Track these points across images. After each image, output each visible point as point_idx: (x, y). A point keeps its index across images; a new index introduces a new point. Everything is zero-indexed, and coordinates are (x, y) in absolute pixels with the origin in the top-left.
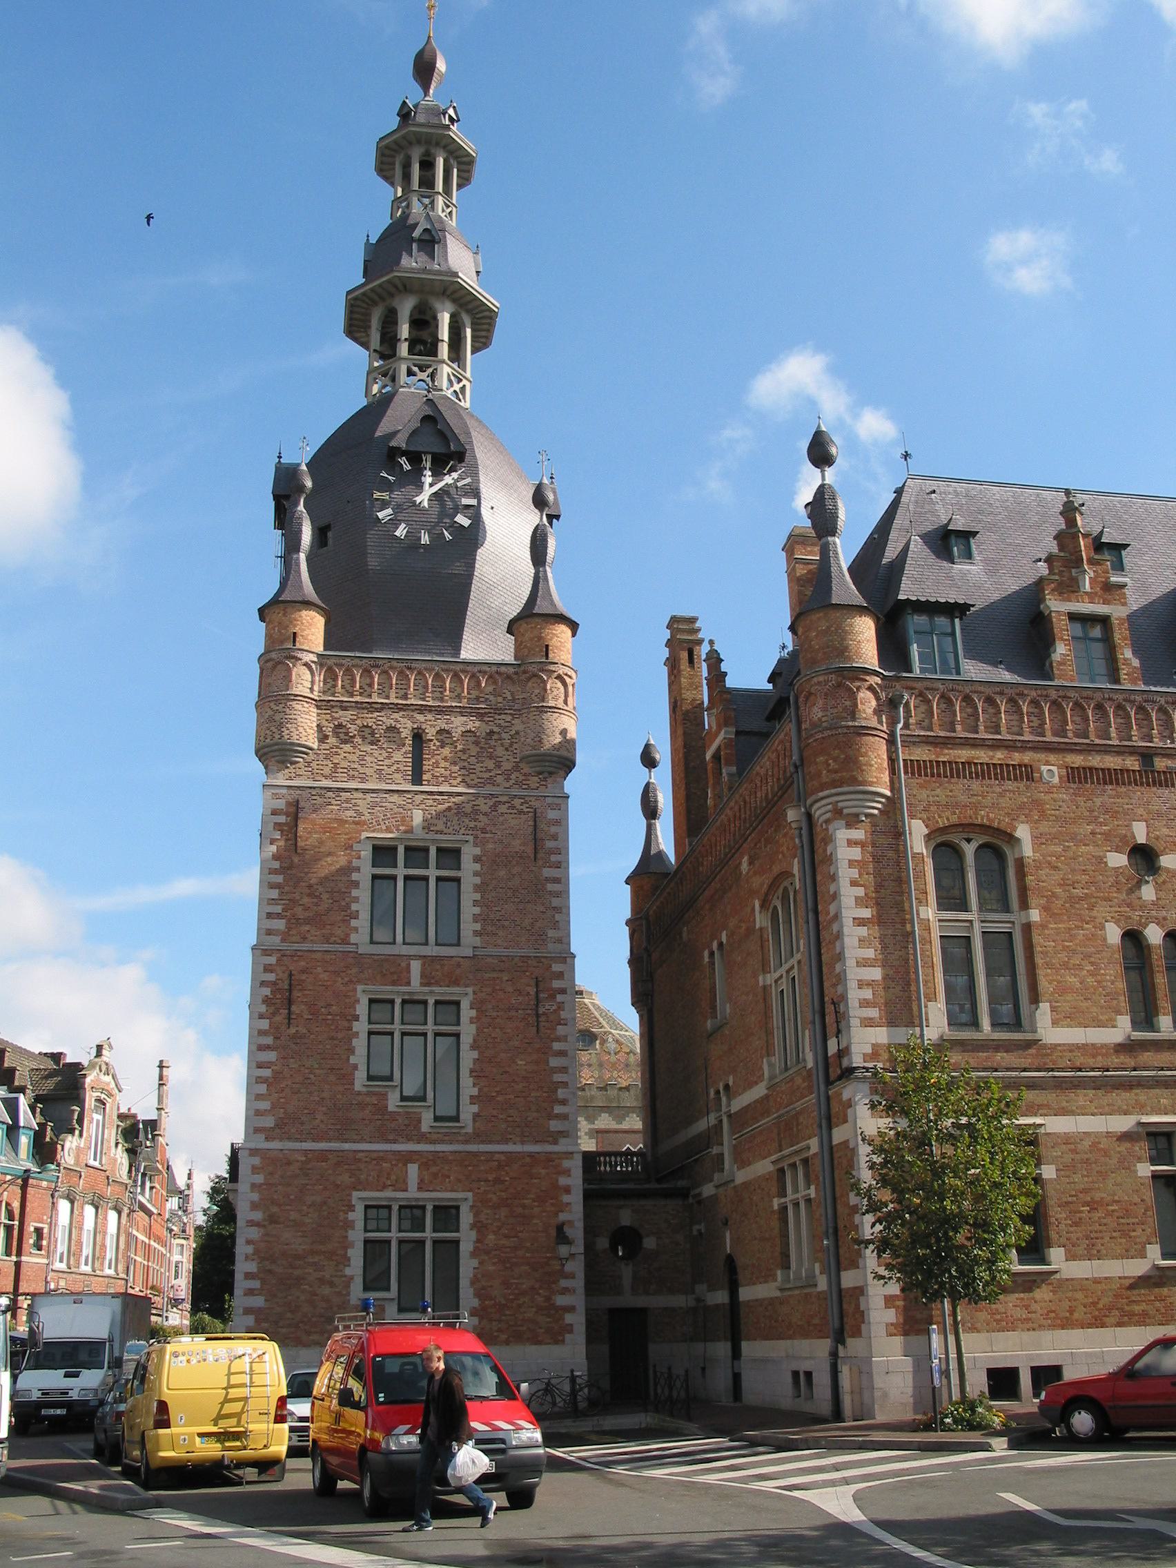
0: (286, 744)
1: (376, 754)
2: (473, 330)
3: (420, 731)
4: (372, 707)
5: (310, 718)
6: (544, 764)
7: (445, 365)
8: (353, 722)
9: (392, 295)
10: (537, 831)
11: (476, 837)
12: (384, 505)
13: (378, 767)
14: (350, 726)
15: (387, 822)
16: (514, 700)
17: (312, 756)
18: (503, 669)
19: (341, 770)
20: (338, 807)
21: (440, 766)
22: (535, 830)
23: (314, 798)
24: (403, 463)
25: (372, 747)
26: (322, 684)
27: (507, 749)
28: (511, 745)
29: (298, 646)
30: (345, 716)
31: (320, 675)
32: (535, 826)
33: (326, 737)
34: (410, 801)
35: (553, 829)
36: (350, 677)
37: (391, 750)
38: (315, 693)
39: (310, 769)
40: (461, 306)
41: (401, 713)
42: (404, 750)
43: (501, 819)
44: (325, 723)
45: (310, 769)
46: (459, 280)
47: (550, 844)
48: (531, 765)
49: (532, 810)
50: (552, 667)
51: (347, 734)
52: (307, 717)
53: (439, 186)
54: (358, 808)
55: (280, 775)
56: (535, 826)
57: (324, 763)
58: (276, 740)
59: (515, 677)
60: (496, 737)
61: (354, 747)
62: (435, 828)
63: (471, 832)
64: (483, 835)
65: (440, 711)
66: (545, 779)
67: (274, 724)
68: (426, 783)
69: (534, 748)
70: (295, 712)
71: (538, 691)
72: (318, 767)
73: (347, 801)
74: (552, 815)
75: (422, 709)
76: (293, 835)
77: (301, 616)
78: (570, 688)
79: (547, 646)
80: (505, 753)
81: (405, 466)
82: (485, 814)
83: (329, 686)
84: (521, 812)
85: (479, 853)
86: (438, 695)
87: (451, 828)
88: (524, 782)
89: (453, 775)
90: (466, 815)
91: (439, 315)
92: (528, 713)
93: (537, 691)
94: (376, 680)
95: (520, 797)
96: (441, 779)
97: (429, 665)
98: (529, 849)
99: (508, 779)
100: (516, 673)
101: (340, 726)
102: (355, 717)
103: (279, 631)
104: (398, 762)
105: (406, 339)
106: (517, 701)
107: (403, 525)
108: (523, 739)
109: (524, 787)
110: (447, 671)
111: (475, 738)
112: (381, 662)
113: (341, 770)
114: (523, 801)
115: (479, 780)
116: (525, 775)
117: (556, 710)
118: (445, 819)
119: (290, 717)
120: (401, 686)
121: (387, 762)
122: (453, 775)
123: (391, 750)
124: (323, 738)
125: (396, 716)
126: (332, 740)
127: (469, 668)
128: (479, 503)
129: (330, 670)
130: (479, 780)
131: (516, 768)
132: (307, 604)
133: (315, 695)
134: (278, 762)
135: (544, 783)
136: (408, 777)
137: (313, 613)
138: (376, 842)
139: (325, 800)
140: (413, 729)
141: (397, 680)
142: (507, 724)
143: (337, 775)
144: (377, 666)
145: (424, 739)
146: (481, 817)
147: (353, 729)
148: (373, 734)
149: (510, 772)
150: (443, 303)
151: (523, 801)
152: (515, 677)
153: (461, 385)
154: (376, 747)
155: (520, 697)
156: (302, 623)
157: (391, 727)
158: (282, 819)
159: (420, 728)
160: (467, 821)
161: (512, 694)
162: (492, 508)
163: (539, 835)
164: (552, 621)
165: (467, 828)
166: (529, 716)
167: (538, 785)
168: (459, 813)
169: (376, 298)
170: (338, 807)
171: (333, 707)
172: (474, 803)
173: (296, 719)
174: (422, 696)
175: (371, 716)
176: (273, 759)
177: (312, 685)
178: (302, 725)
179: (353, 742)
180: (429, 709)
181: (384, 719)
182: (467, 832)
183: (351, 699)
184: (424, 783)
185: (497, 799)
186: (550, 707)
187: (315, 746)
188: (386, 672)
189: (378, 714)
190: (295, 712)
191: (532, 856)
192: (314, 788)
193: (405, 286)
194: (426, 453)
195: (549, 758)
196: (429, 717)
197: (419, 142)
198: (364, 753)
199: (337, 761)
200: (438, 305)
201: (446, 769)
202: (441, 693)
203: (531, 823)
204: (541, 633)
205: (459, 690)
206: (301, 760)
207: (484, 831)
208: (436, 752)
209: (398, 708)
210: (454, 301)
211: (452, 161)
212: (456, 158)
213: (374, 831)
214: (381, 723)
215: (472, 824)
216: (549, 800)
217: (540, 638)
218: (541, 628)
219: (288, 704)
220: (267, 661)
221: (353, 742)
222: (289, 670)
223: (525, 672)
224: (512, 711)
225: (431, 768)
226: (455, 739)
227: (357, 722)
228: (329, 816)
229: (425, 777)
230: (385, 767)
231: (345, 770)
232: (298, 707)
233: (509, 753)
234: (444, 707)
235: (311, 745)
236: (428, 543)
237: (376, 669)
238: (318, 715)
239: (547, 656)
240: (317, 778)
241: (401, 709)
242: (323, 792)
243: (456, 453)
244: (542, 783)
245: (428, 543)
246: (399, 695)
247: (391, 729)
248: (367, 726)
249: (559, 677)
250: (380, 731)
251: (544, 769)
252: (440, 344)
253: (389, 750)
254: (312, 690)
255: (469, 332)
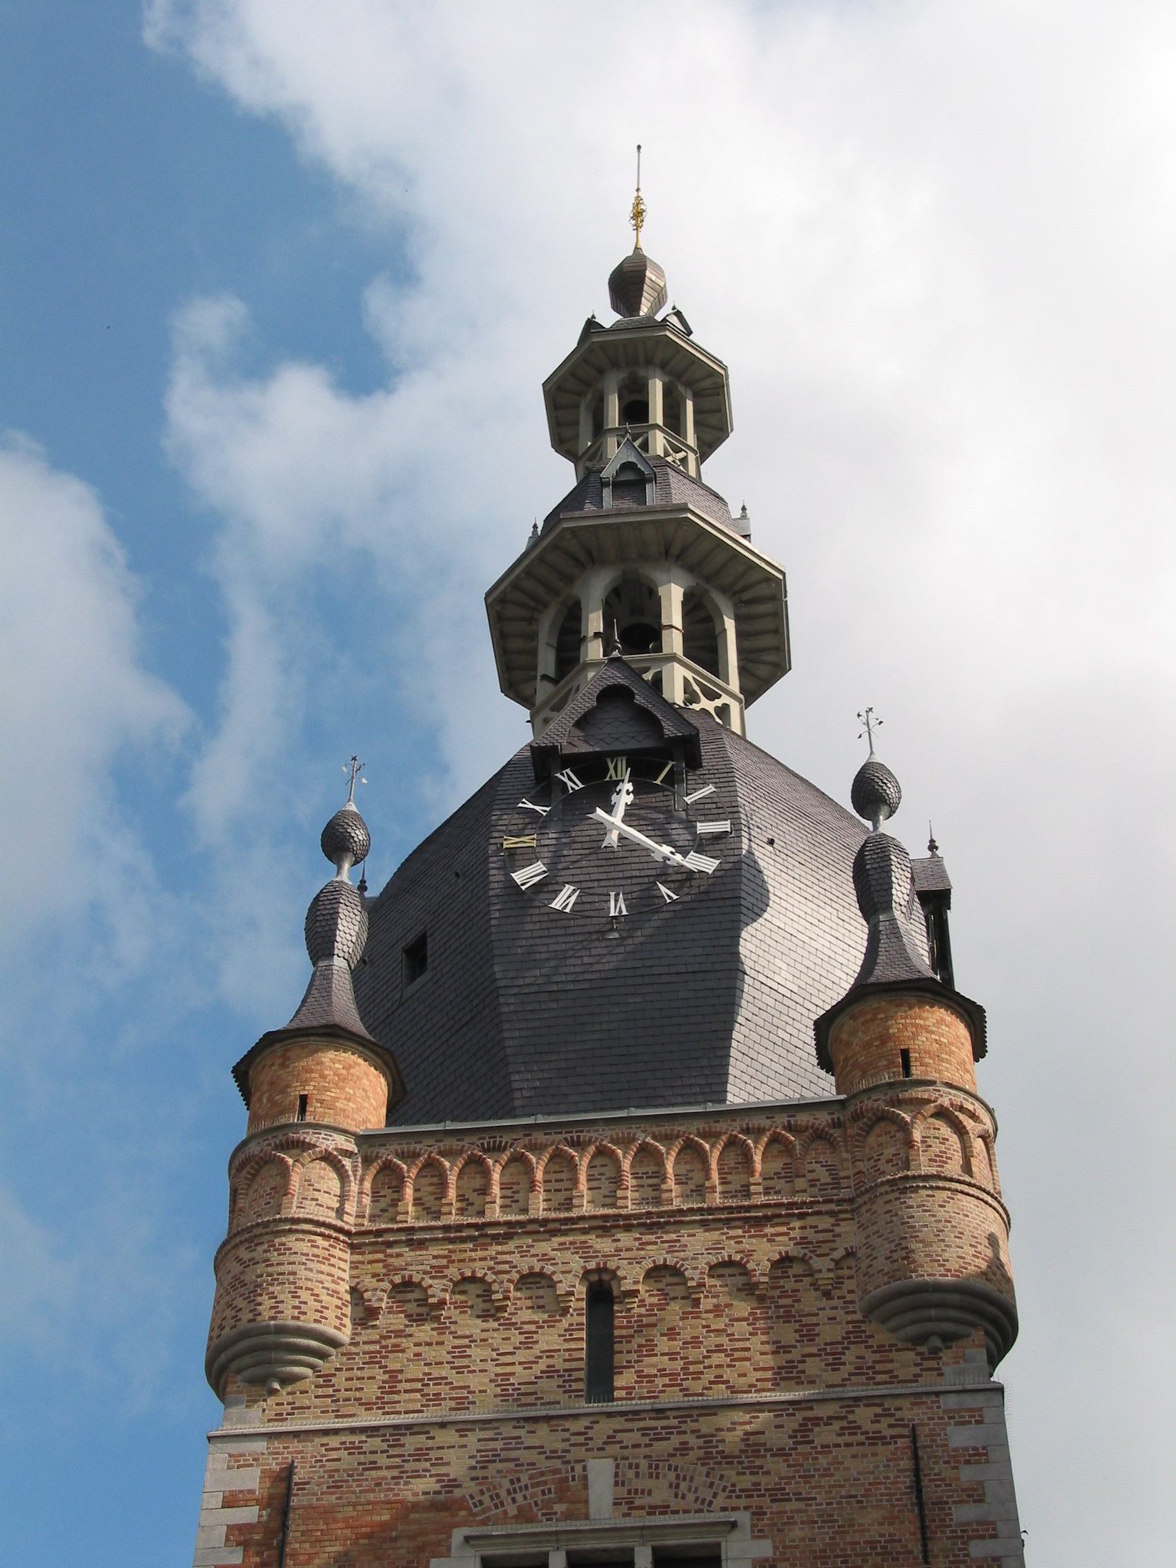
0: (266, 1331)
1: (496, 1338)
2: (738, 619)
3: (606, 1277)
4: (483, 1234)
5: (334, 1271)
6: (925, 1313)
7: (676, 665)
8: (438, 1272)
9: (570, 580)
10: (925, 1482)
11: (758, 1513)
12: (529, 857)
13: (499, 1370)
14: (430, 1282)
15: (519, 1497)
16: (836, 1183)
17: (336, 1359)
18: (803, 1118)
19: (408, 1386)
20: (395, 1473)
21: (657, 1350)
22: (918, 1481)
23: (334, 1455)
24: (565, 779)
25: (485, 1325)
26: (367, 1200)
27: (827, 1295)
28: (839, 1281)
29: (309, 1119)
30: (415, 1263)
31: (362, 1180)
32: (917, 1472)
33: (372, 1313)
34: (581, 1439)
35: (967, 1474)
36: (435, 1180)
37: (532, 1328)
38: (346, 1217)
39: (330, 1391)
40: (708, 579)
41: (557, 1240)
42: (565, 1323)
43: (823, 1461)
44: (369, 1282)
45: (330, 1391)
46: (689, 515)
47: (964, 1513)
48: (893, 1323)
49: (906, 1432)
50: (919, 1093)
51: (423, 1302)
52: (325, 1268)
53: (657, 413)
54: (443, 1470)
55: (255, 1411)
56: (917, 1472)
57: (366, 1373)
58: (243, 1325)
59: (836, 1133)
60: (797, 1269)
61: (441, 1331)
62: (646, 1501)
63: (742, 1502)
64: (776, 1507)
65: (652, 1224)
66: (935, 1352)
67: (242, 1290)
68: (623, 1393)
69: (893, 1277)
70: (292, 1258)
71: (892, 1150)
72: (349, 1384)
73: (420, 1454)
74: (959, 1437)
75: (606, 1226)
76: (274, 1552)
77: (321, 1063)
78: (978, 1145)
79: (905, 1054)
80: (824, 1302)
81: (570, 784)
82: (781, 1453)
83: (383, 1203)
84: (876, 1439)
85: (770, 1554)
86: (649, 1193)
87: (691, 1497)
88: (879, 1367)
89: (692, 1368)
90: (728, 1459)
91: (662, 591)
92: (872, 1201)
93: (889, 1151)
94: (496, 1176)
95: (870, 1401)
96: (660, 1382)
97: (621, 1131)
98: (908, 1530)
99: (835, 1365)
100: (837, 1124)
101: (408, 1285)
102: (444, 1262)
103: (270, 1099)
104: (550, 1353)
105: (597, 635)
106: (844, 1183)
107: (568, 889)
108: (864, 1265)
109: (879, 1378)
110: (667, 1139)
111: (743, 1279)
112: (506, 1139)
113: (408, 1386)
114: (879, 1410)
115: (759, 1375)
116: (880, 1349)
117: (941, 1184)
118: (672, 1476)
119: (280, 1269)
120: (558, 1185)
121: (522, 1355)
122: (692, 1368)
123: (532, 1328)
124: (365, 1315)
125: (544, 1247)
126: (390, 1320)
127: (722, 1126)
128: (736, 825)
129: (388, 1168)
130: (759, 1375)
131: (855, 1336)
132: (335, 1035)
133: (349, 1222)
134: (252, 1381)
135: (933, 1364)
136: (575, 1386)
137: (350, 1057)
138: (490, 1552)
139: (362, 1458)
140: (587, 1273)
141: (546, 1172)
142: (821, 1237)
143: (396, 1397)
144: (498, 1149)
145: (615, 1293)
146: (770, 1463)
147: (438, 1289)
148: (486, 1294)
149: (839, 1348)
150: (668, 571)
151: (879, 1410)
152: (836, 1133)
153: (718, 702)
154: (496, 1325)
155: (850, 1172)
156: (323, 1077)
157: (532, 1274)
158: (248, 1514)
159: (605, 1270)
160: (731, 1473)
161: (831, 1169)
162: (771, 842)
163: (931, 1491)
164: (913, 1001)
165: (732, 1491)
166: (875, 1207)
167: (917, 1370)
168: (708, 1456)
169: (540, 591)
170: (395, 1473)
171: (390, 1244)
172: (748, 1427)
173: (294, 1273)
174: (609, 1201)
175: (480, 1254)
176: (239, 1378)
177: (342, 1203)
178: (309, 1284)
179: (437, 1318)
180: (626, 1223)
181: (515, 1258)
182: (735, 1502)
183: (433, 1223)
184: (617, 1394)
185: (809, 1414)
186: (926, 1178)
187: (345, 1335)
188: (519, 1159)
189: (499, 1248)
190: (292, 1258)
191: (917, 1549)
192: (336, 1432)
193: (590, 554)
194: (614, 754)
195: (936, 1297)
196: (626, 1239)
197: (615, 365)
198: (466, 1341)
199: (397, 1366)
200: (657, 575)
201: (672, 1356)
202: (656, 1187)
203: (906, 1463)
204: (888, 1028)
205: (698, 1177)
206: (309, 1371)
207: (777, 1495)
208: (645, 1320)
209: (546, 1228)
210: (691, 569)
211: (681, 388)
212: (689, 384)
213: (484, 1523)
214: (506, 1267)
215: (746, 1481)
216: (950, 1402)
217: (885, 1039)
218: (886, 1019)
219: (277, 1241)
220: (241, 1168)
221: (437, 1318)
222: (285, 1173)
223: (856, 1117)
224: (833, 1207)
225: (634, 1356)
226: (690, 1284)
227: (447, 1272)
228: (371, 1496)
229: (619, 1381)
230: (518, 1369)
231: (419, 1385)
232: (304, 1247)
233: (835, 1302)
234: (661, 1215)
235: (331, 1331)
236: (625, 913)
237: (496, 1154)
238: (355, 1265)
239: (907, 1072)
240: (343, 1411)
241: (554, 1233)
242: (356, 1439)
243: (675, 740)
244: (926, 1364)
245: (625, 913)
246: (555, 1204)
247: (534, 1280)
248: (473, 1279)
249: (942, 1114)
250: (504, 1286)
251: (930, 1326)
252: (665, 633)
253: (527, 1328)
254: (340, 1212)
255: (730, 625)
